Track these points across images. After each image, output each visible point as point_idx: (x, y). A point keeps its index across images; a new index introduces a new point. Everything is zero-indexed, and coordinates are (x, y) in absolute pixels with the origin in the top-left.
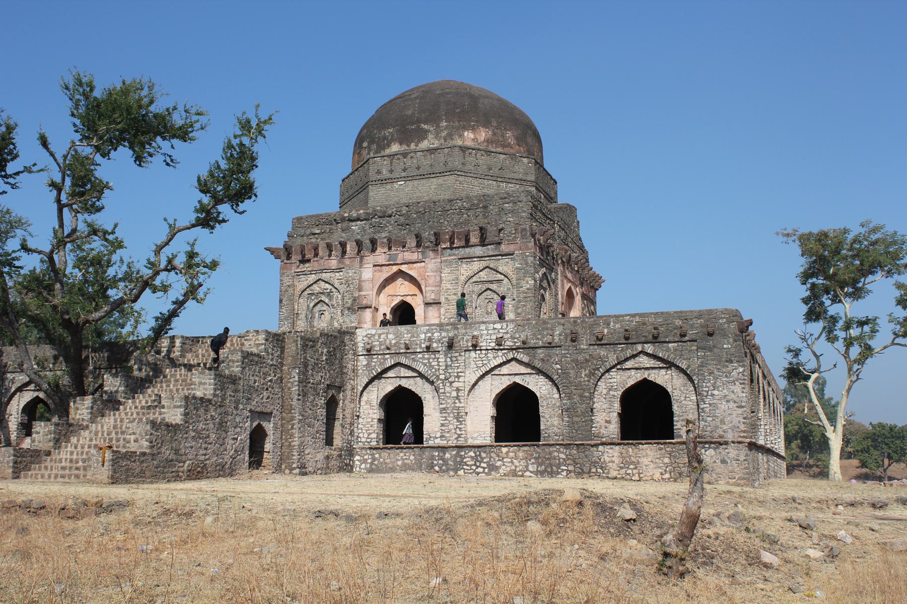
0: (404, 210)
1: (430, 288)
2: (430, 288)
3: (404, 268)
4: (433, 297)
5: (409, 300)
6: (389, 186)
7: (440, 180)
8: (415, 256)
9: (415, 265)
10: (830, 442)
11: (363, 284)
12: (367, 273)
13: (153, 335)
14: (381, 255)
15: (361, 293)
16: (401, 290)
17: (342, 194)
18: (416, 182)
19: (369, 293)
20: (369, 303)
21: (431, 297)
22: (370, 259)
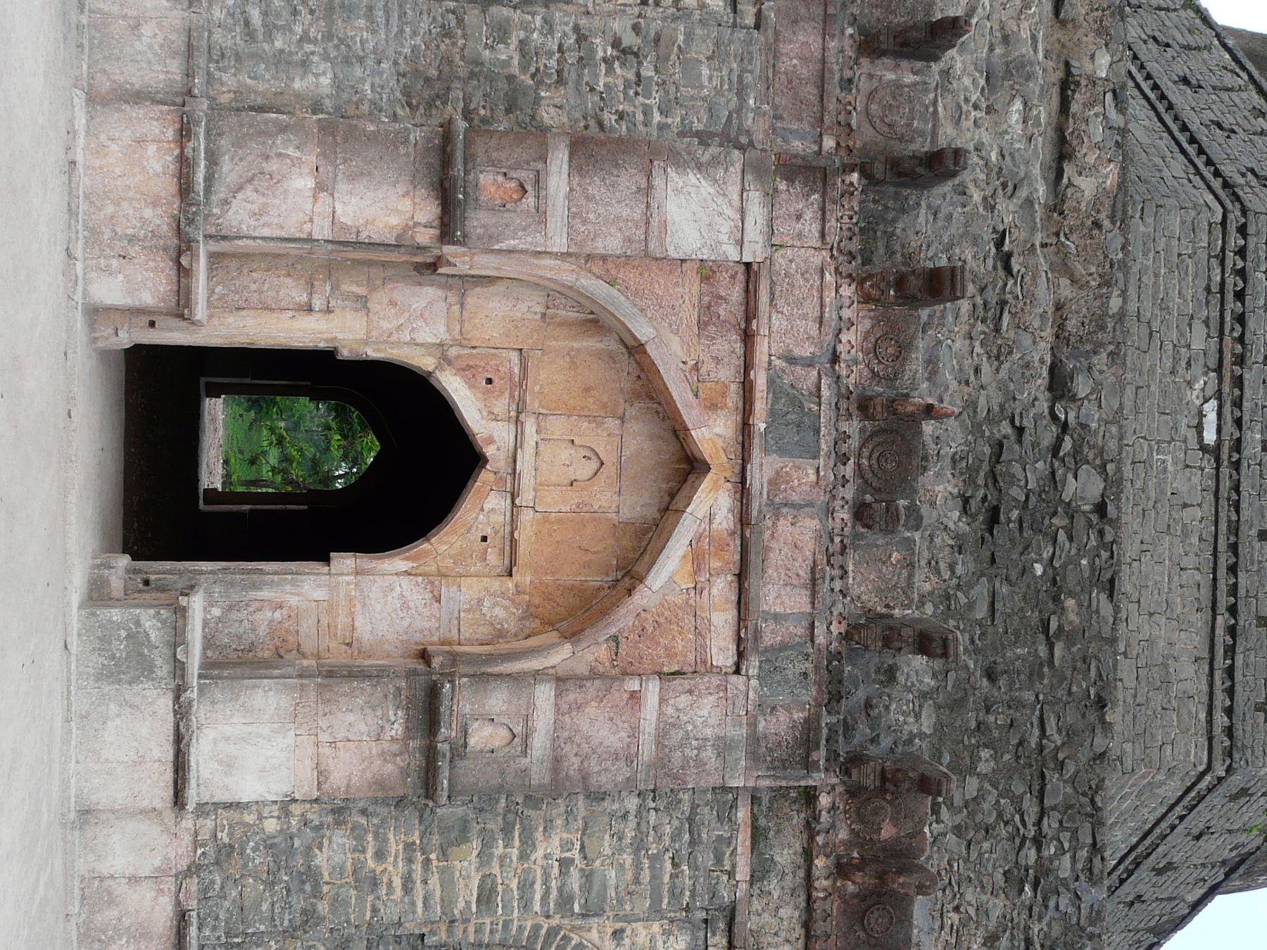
0: (1084, 487)
1: (543, 720)
2: (543, 720)
3: (711, 504)
4: (482, 736)
5: (482, 508)
6: (1199, 339)
7: (1190, 677)
8: (781, 596)
9: (722, 588)
10: (345, 354)
11: (628, 180)
12: (701, 213)
13: (800, 178)
14: (811, 316)
15: (559, 160)
16: (545, 463)
17: (1225, 28)
18: (1197, 517)
19: (553, 218)
20: (477, 221)
21: (485, 723)
22: (799, 241)
